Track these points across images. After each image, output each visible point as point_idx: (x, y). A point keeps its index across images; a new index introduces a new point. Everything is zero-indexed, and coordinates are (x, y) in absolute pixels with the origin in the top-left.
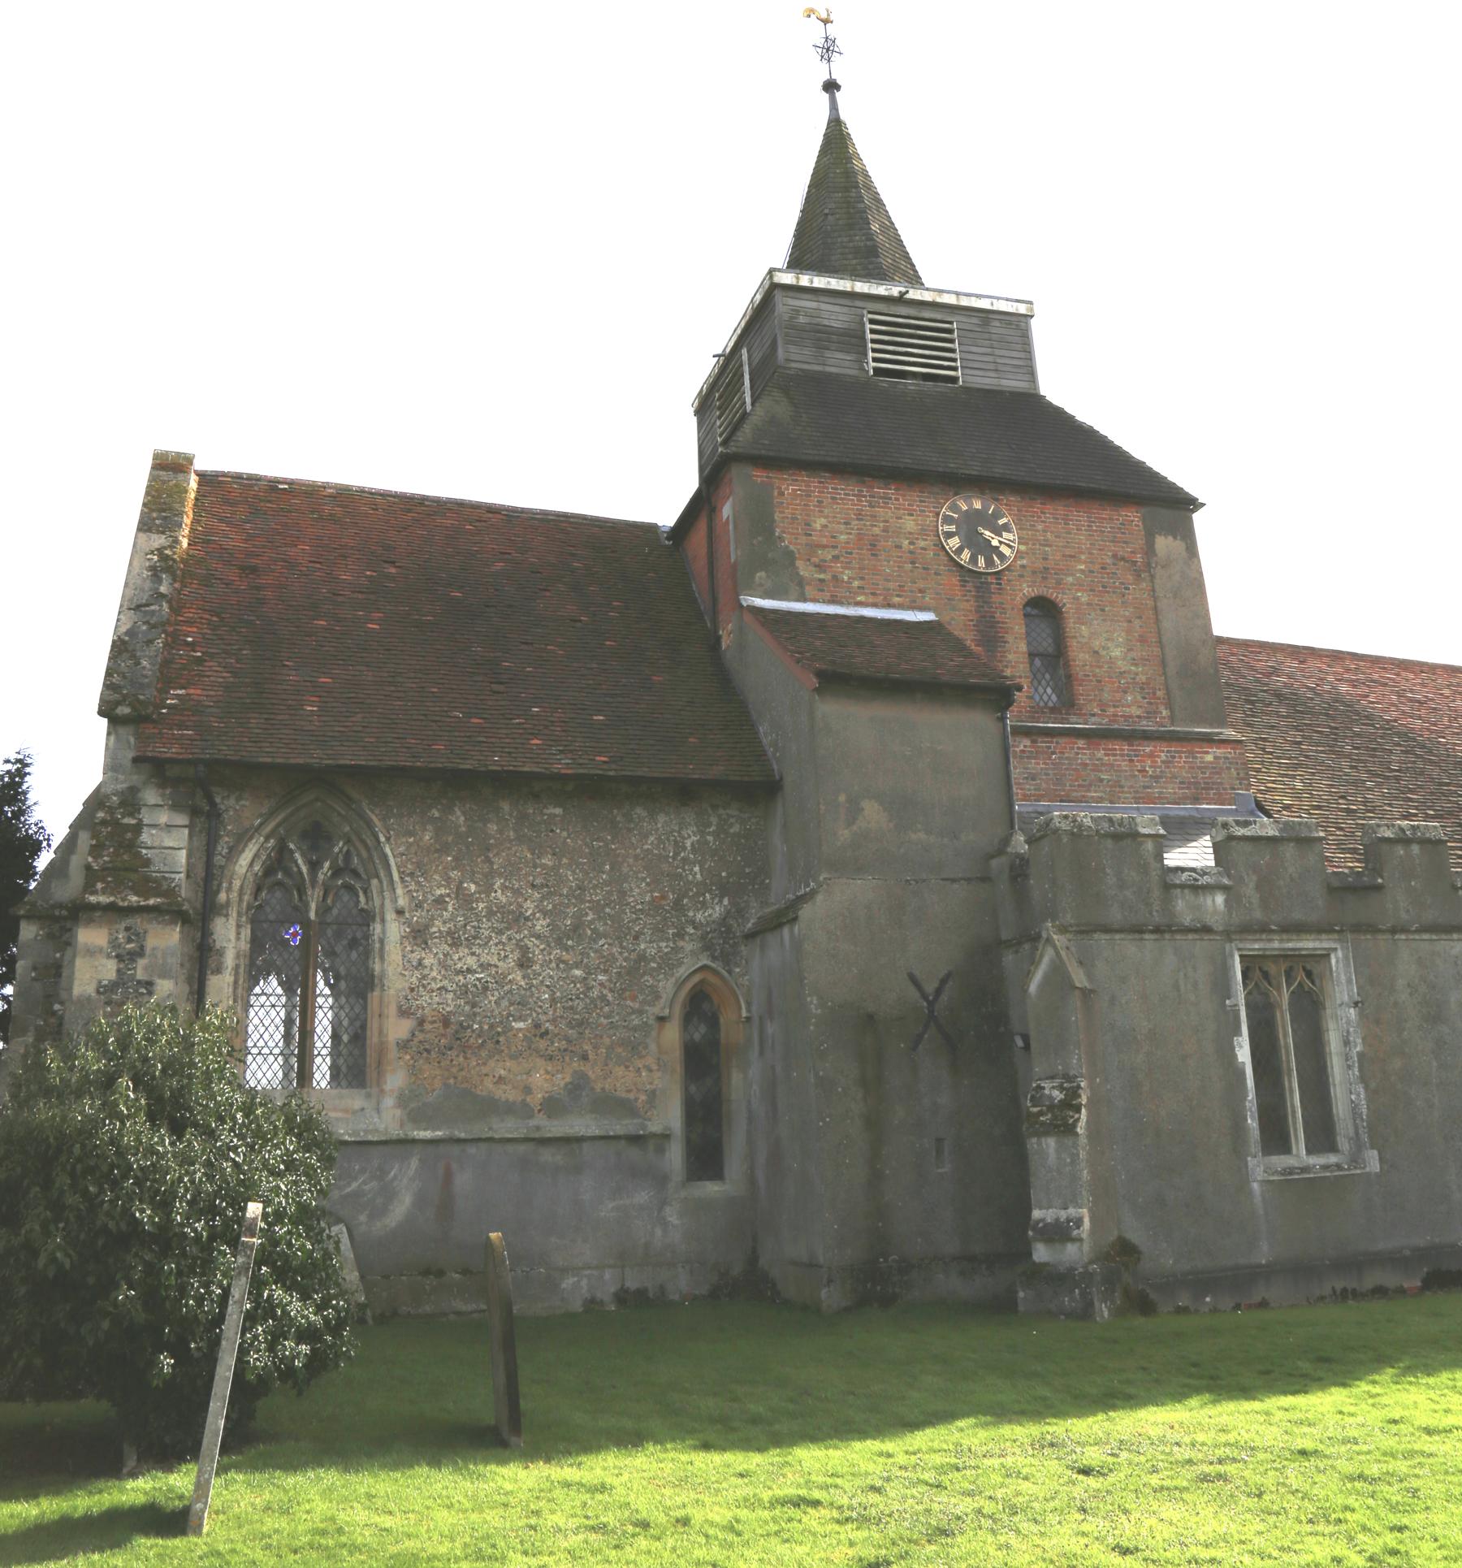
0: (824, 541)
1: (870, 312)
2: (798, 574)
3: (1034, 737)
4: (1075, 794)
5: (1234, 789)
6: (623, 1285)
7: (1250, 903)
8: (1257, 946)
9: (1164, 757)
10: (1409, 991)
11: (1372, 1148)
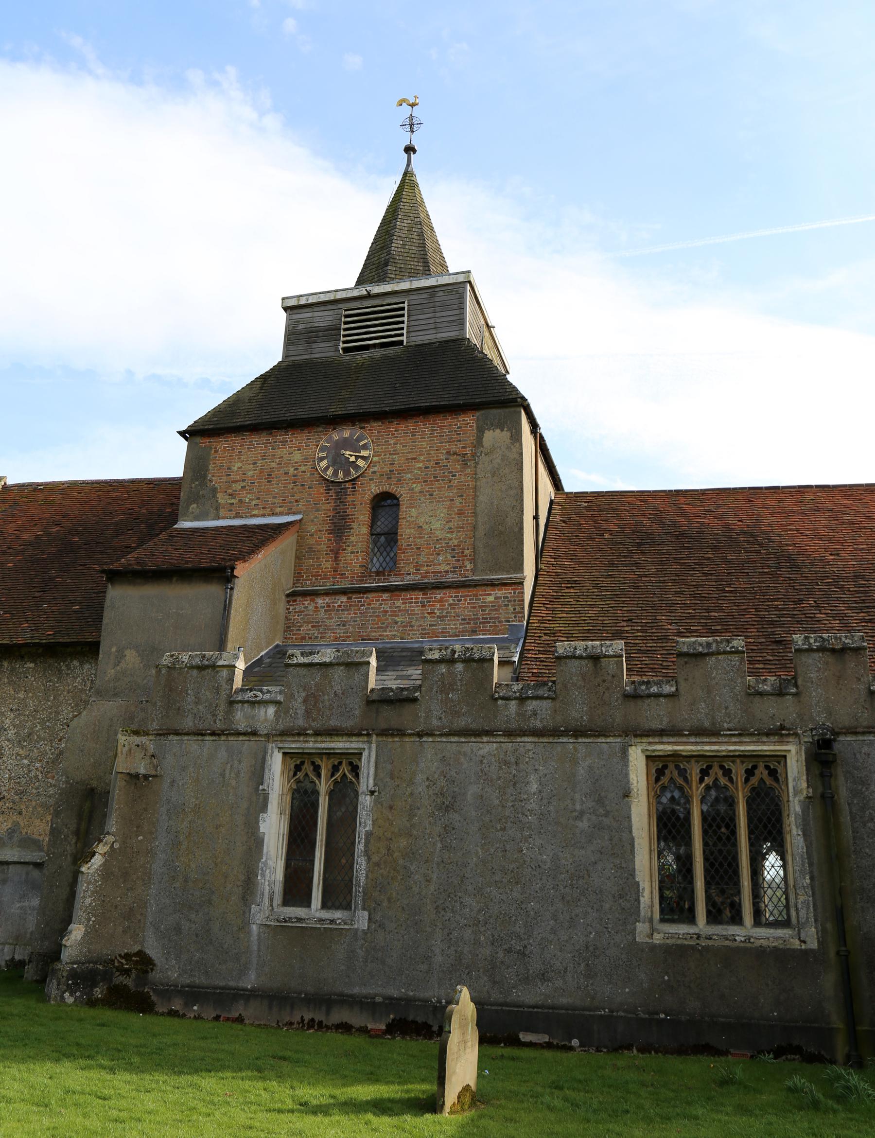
0: (238, 478)
1: (346, 310)
2: (217, 502)
3: (350, 595)
4: (374, 634)
5: (509, 621)
6: (13, 957)
7: (296, 713)
8: (293, 746)
9: (451, 601)
10: (427, 784)
11: (364, 909)
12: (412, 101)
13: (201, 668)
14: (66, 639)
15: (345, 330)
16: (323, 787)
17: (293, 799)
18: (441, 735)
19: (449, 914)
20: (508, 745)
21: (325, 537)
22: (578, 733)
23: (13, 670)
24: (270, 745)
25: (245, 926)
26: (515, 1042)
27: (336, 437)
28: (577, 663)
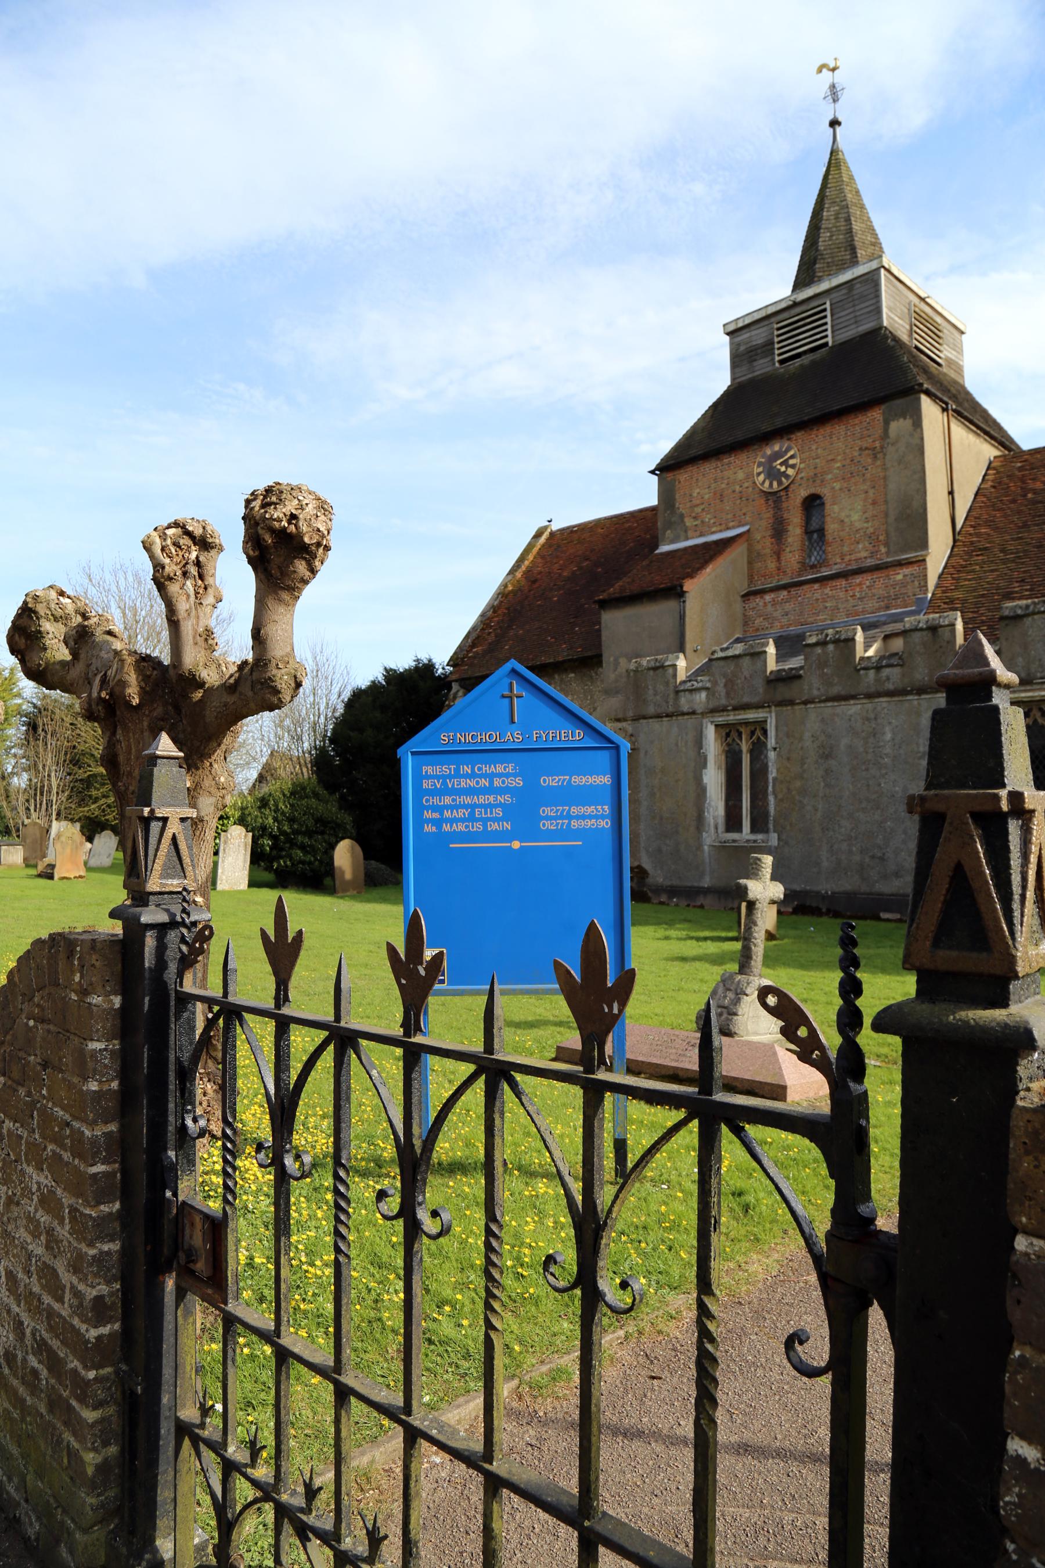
0: (698, 502)
9: (868, 583)
11: (775, 831)
12: (832, 65)
13: (655, 669)
14: (589, 654)
15: (779, 342)
16: (745, 747)
17: (727, 757)
18: (820, 702)
19: (831, 833)
20: (869, 705)
21: (768, 541)
23: (562, 680)
24: (705, 721)
25: (700, 847)
26: (879, 919)
27: (769, 452)
28: (918, 634)
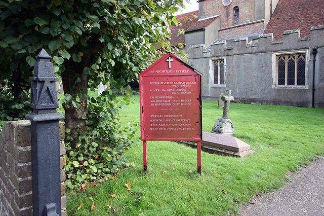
16: (219, 65)
22: (263, 52)
